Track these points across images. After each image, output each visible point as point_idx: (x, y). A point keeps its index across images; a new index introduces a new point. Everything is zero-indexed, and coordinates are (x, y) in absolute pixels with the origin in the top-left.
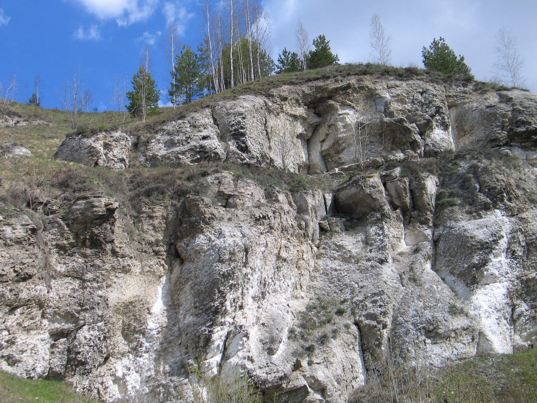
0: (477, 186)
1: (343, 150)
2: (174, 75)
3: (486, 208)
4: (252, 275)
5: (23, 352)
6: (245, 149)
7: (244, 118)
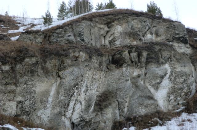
0: (161, 56)
1: (116, 40)
2: (59, 10)
3: (163, 63)
4: (84, 84)
5: (8, 107)
6: (83, 40)
7: (83, 29)
